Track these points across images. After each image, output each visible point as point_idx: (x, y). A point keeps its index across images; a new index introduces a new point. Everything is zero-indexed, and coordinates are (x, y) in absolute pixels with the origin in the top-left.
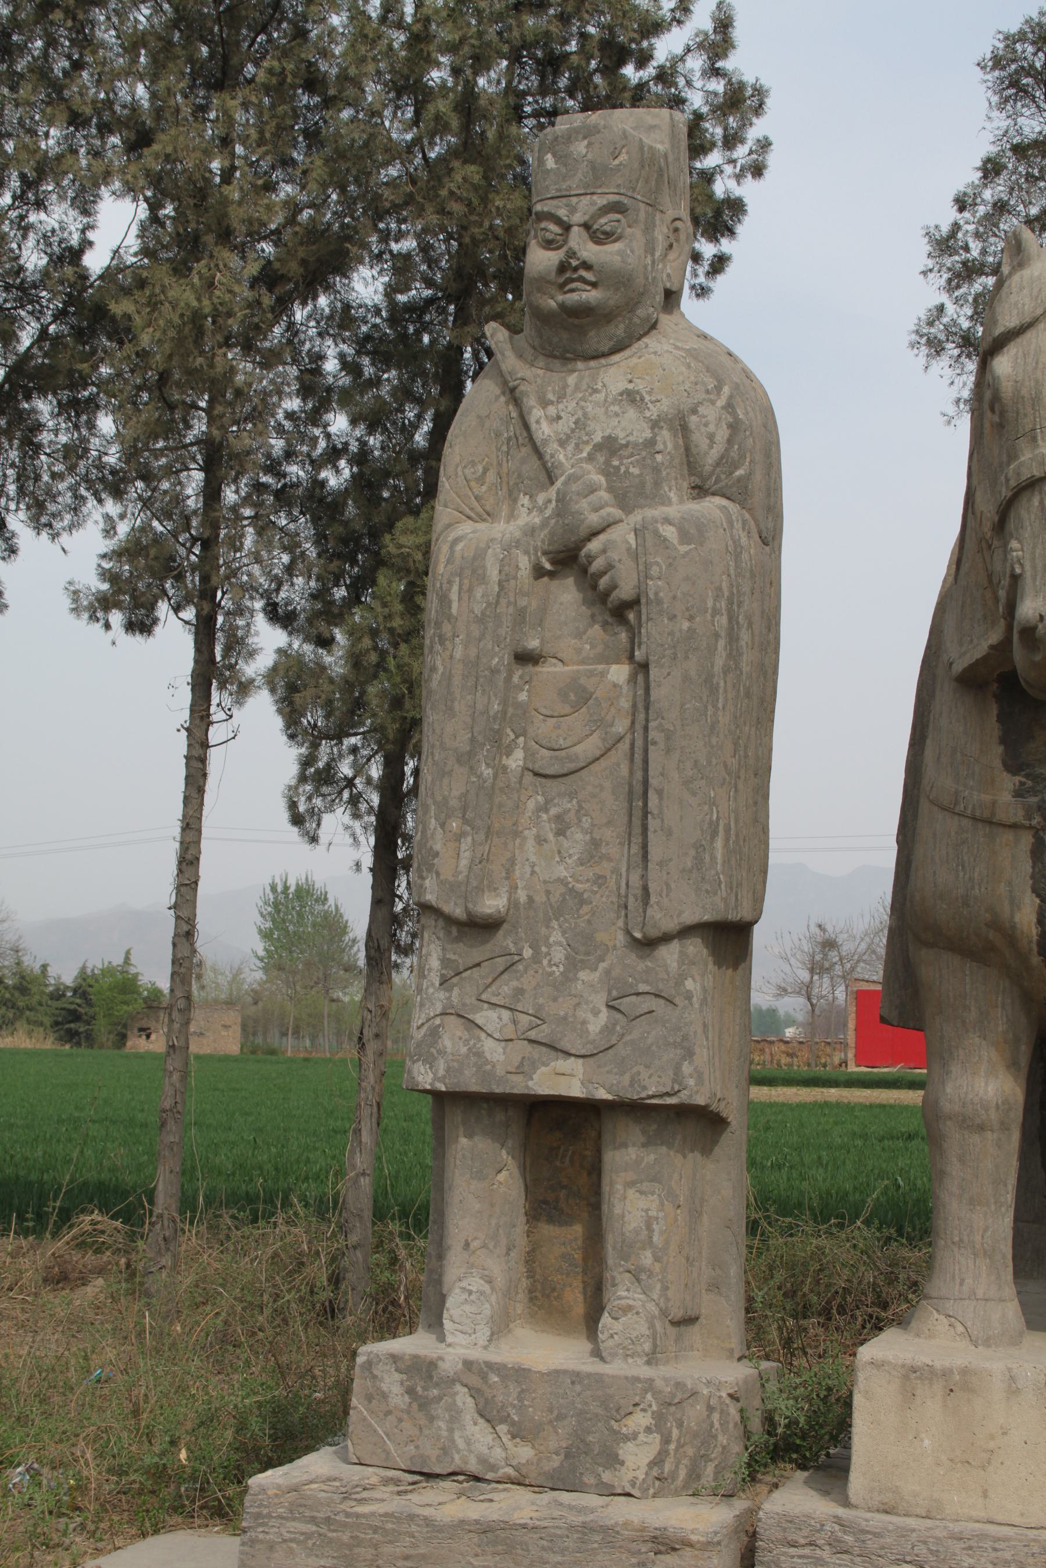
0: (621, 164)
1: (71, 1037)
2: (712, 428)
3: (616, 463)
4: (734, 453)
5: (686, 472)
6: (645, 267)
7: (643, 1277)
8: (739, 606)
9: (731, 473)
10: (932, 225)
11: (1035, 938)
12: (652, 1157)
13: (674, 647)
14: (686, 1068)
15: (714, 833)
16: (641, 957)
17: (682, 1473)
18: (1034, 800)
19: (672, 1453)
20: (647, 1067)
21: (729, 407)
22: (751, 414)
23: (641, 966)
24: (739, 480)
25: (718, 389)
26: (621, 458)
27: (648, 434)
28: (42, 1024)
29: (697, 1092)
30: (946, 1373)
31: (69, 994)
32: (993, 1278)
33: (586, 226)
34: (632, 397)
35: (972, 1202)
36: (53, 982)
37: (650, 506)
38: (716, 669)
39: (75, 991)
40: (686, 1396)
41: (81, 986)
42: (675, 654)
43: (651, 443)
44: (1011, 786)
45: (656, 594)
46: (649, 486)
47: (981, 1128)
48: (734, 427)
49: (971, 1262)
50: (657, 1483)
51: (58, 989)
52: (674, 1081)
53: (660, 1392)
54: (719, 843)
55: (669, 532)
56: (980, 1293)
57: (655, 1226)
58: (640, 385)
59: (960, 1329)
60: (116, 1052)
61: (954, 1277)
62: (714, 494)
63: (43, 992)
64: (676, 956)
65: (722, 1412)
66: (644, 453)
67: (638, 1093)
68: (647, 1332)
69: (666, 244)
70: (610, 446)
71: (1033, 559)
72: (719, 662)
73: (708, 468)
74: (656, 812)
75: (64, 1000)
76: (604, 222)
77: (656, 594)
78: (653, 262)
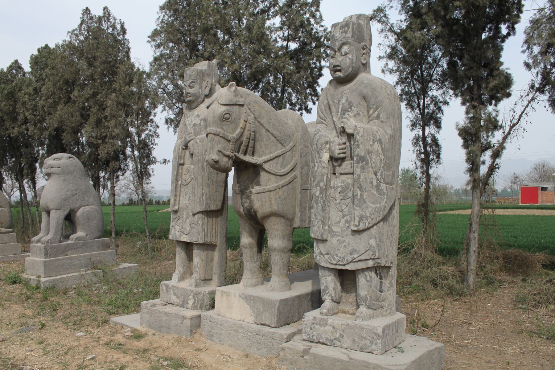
14: (199, 237)
15: (203, 195)
30: (226, 292)
33: (189, 86)
34: (198, 116)
43: (200, 124)
47: (246, 248)
54: (204, 197)
55: (198, 141)
58: (199, 113)
70: (195, 125)
76: (191, 85)
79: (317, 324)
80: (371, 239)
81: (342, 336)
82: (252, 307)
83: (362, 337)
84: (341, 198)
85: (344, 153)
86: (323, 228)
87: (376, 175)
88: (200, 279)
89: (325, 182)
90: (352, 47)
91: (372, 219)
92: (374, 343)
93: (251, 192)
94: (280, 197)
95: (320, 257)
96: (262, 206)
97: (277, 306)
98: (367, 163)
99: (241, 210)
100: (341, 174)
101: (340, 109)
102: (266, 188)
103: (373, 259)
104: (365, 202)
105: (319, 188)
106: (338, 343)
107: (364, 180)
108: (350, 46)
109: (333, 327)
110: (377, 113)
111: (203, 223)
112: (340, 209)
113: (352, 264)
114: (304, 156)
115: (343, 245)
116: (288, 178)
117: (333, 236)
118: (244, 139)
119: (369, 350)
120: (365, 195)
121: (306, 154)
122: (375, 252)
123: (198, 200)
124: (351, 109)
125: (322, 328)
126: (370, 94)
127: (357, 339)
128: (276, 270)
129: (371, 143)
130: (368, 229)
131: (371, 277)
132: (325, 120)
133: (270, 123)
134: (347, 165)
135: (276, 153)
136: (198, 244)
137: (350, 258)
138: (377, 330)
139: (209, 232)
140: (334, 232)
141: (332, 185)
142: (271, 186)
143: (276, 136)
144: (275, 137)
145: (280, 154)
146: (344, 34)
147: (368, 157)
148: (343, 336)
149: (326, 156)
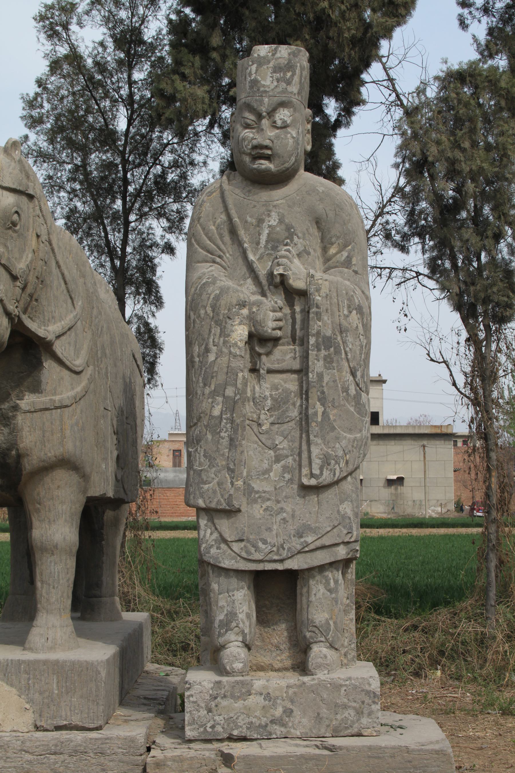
10: (25, 93)
79: (225, 696)
80: (342, 502)
81: (289, 712)
82: (24, 691)
83: (336, 705)
84: (271, 420)
85: (280, 329)
86: (232, 483)
87: (353, 374)
90: (297, 115)
91: (347, 462)
92: (366, 712)
93: (16, 408)
94: (77, 424)
97: (103, 674)
98: (337, 352)
100: (270, 371)
101: (264, 238)
102: (57, 398)
103: (348, 543)
104: (333, 429)
105: (220, 399)
106: (278, 730)
107: (331, 384)
108: (295, 110)
109: (268, 697)
110: (345, 254)
112: (269, 443)
113: (299, 556)
115: (279, 517)
117: (255, 501)
119: (355, 730)
120: (332, 414)
122: (351, 528)
124: (292, 240)
125: (240, 704)
126: (331, 215)
127: (324, 712)
128: (53, 600)
129: (346, 312)
130: (337, 482)
131: (336, 582)
132: (220, 257)
134: (285, 354)
135: (68, 319)
137: (296, 544)
138: (370, 685)
140: (258, 492)
141: (249, 394)
143: (67, 279)
144: (66, 283)
146: (284, 85)
147: (339, 338)
148: (292, 711)
149: (240, 332)
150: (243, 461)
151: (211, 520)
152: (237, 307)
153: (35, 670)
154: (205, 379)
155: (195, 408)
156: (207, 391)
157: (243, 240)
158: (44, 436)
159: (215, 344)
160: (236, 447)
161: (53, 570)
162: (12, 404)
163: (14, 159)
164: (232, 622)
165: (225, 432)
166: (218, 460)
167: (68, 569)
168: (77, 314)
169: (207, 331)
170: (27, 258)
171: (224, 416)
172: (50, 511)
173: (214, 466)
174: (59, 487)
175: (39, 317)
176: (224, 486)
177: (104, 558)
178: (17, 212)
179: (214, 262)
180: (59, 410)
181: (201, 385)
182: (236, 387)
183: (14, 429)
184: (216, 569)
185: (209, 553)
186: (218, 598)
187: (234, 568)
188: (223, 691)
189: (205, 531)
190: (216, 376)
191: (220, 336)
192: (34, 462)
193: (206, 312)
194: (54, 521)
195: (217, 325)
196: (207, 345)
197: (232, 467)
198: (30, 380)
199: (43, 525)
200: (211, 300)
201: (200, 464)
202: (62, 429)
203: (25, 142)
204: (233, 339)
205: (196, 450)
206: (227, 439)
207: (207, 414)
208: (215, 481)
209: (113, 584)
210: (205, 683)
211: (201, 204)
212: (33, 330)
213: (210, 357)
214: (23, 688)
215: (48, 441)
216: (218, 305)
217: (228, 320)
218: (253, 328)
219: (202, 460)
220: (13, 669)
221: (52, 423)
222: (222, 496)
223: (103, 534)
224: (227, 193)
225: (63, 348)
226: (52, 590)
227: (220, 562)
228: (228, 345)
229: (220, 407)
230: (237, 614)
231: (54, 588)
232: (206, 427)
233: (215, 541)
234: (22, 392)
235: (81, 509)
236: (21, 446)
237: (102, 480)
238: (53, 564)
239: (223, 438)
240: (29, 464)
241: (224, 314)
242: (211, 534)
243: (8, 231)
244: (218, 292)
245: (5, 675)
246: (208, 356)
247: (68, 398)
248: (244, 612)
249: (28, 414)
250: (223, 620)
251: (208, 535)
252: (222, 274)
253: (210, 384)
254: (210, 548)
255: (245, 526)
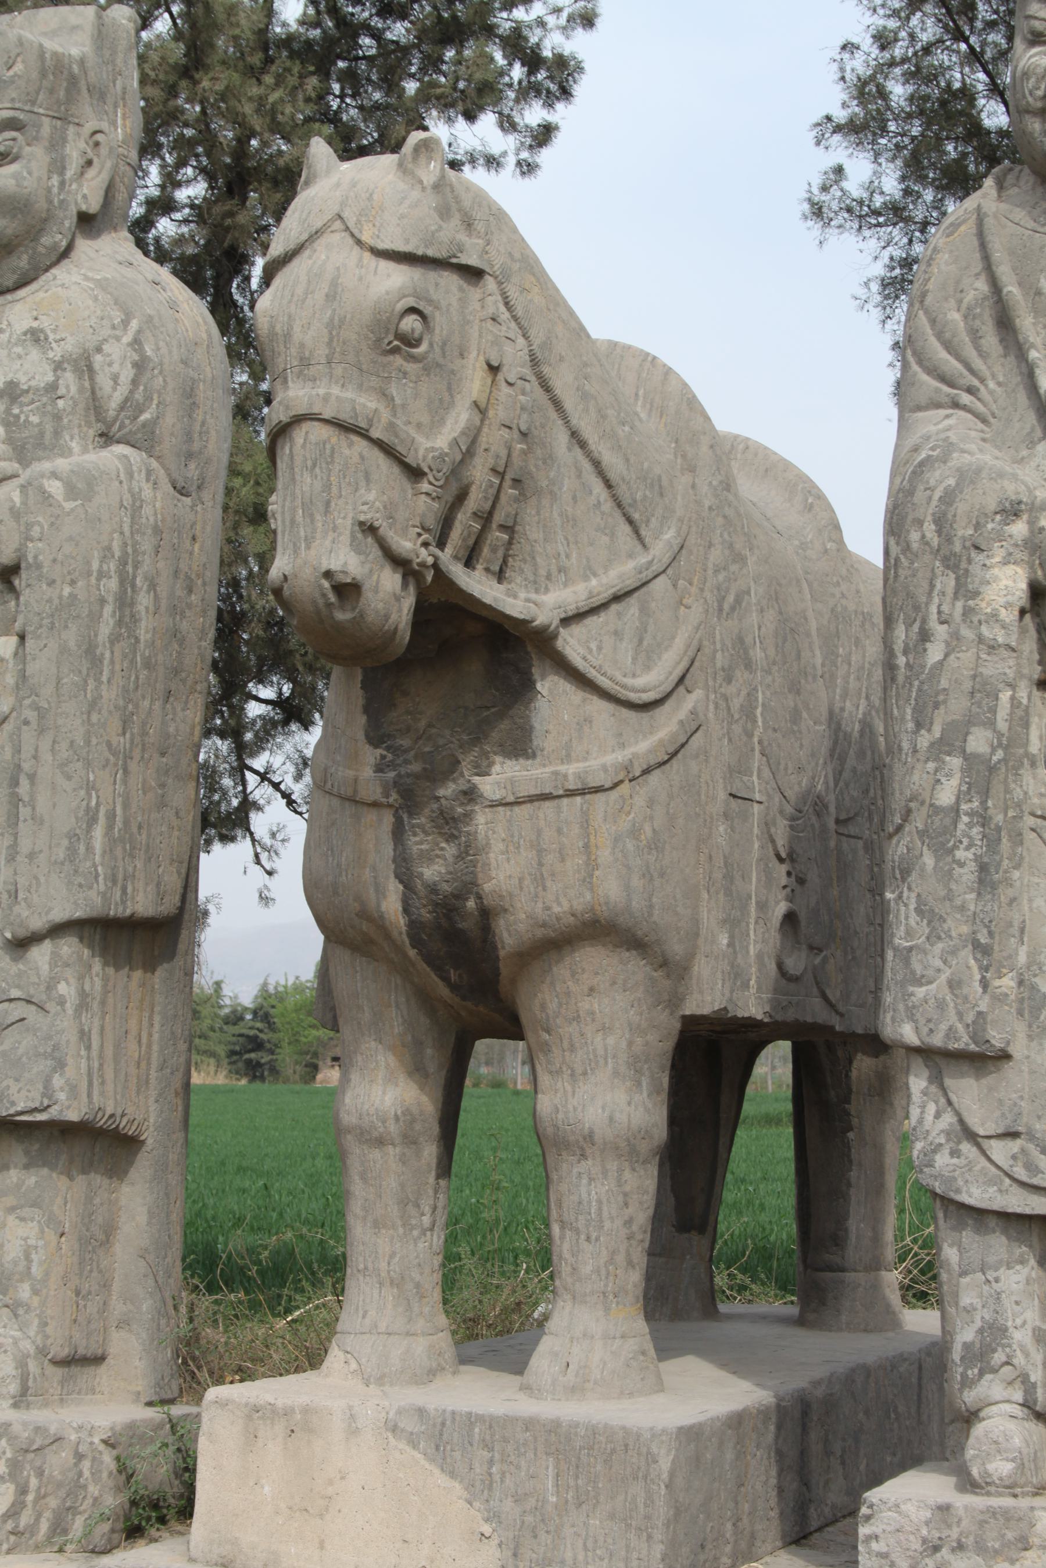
0: (16, 75)
1: (254, 1071)
2: (116, 368)
3: (16, 411)
4: (139, 396)
5: (93, 418)
6: (49, 190)
7: (21, 1311)
8: (136, 568)
9: (136, 418)
11: (404, 929)
12: (33, 1180)
13: (52, 616)
14: (57, 1081)
15: (93, 820)
16: (15, 960)
17: (44, 1527)
18: (391, 775)
19: (30, 1505)
20: (17, 1080)
21: (136, 343)
22: (164, 350)
23: (15, 968)
24: (144, 425)
25: (125, 323)
26: (22, 405)
27: (50, 377)
28: (213, 1054)
29: (68, 1107)
30: (288, 1412)
31: (249, 1017)
32: (400, 1309)
34: (36, 336)
35: (376, 1224)
36: (228, 1002)
37: (48, 458)
38: (100, 639)
39: (255, 1013)
40: (47, 1442)
41: (261, 1007)
42: (53, 623)
43: (52, 387)
44: (372, 761)
45: (36, 557)
46: (48, 436)
47: (380, 1142)
48: (140, 366)
49: (376, 1292)
50: (12, 1538)
51: (234, 1012)
52: (44, 1095)
53: (16, 1437)
55: (55, 488)
56: (382, 1327)
57: (34, 1256)
58: (45, 323)
59: (354, 1366)
60: (307, 1087)
61: (357, 1309)
62: (118, 442)
63: (216, 1015)
64: (47, 958)
65: (94, 1459)
66: (45, 399)
67: (7, 1109)
68: (14, 1373)
69: (82, 161)
71: (283, 513)
72: (105, 630)
73: (112, 413)
74: (26, 799)
75: (242, 1024)
77: (36, 557)
78: (62, 183)
79: (960, 1547)
82: (481, 1489)
86: (985, 984)
88: (42, 1351)
89: (1002, 725)
93: (470, 795)
94: (635, 832)
95: (955, 1153)
96: (540, 881)
97: (665, 1464)
99: (391, 905)
102: (571, 769)
105: (955, 762)
111: (83, 994)
114: (733, 609)
116: (666, 725)
118: (479, 473)
121: (738, 601)
123: (61, 854)
128: (587, 1269)
132: (970, 390)
133: (585, 396)
135: (613, 573)
136: (51, 1124)
139: (109, 1052)
142: (594, 763)
143: (612, 476)
144: (608, 485)
145: (631, 583)
150: (1016, 924)
151: (937, 1079)
152: (998, 517)
153: (505, 1440)
154: (918, 710)
155: (896, 786)
156: (924, 740)
157: (1026, 340)
158: (540, 864)
159: (944, 617)
160: (994, 886)
161: (584, 1196)
162: (462, 785)
163: (421, 182)
164: (994, 1351)
165: (967, 849)
166: (950, 923)
167: (625, 1195)
168: (650, 563)
169: (925, 585)
170: (456, 422)
171: (964, 807)
172: (572, 1049)
173: (939, 938)
174: (592, 990)
175: (522, 571)
176: (965, 991)
177: (853, 1174)
178: (412, 310)
179: (956, 405)
180: (578, 799)
181: (910, 725)
182: (994, 731)
183: (468, 846)
184: (951, 1208)
185: (930, 1165)
186: (957, 1285)
187: (995, 1207)
188: (955, 1533)
189: (923, 1107)
190: (945, 702)
191: (956, 597)
192: (522, 927)
193: (923, 537)
194: (585, 1073)
195: (948, 567)
196: (924, 621)
197: (983, 940)
198: (504, 725)
199: (559, 1084)
200: (934, 502)
201: (909, 934)
202: (586, 846)
203: (836, 182)
204: (989, 604)
205: (900, 897)
206: (972, 866)
207: (923, 803)
208: (943, 978)
209: (877, 1239)
210: (909, 1508)
211: (931, 259)
212: (487, 600)
213: (929, 652)
214: (478, 1483)
215: (553, 875)
216: (950, 516)
217: (973, 553)
218: (1040, 573)
219: (912, 923)
220: (456, 1435)
221: (559, 831)
222: (960, 1015)
223: (849, 1114)
224: (989, 222)
225: (593, 646)
226: (584, 1245)
227: (958, 1191)
228: (975, 619)
229: (955, 782)
230: (1006, 1330)
231: (588, 1239)
232: (922, 834)
233: (948, 1133)
234: (486, 755)
235: (669, 1045)
236: (487, 887)
237: (719, 975)
238: (584, 1181)
239: (961, 864)
240: (509, 931)
241: (964, 539)
242: (938, 1115)
243: (391, 358)
244: (952, 482)
245: (437, 1448)
246: (925, 650)
247: (604, 768)
248: (1029, 1327)
249: (500, 809)
250: (973, 1343)
251: (929, 1117)
252: (973, 434)
253: (931, 723)
254: (935, 1151)
255: (1022, 1098)
